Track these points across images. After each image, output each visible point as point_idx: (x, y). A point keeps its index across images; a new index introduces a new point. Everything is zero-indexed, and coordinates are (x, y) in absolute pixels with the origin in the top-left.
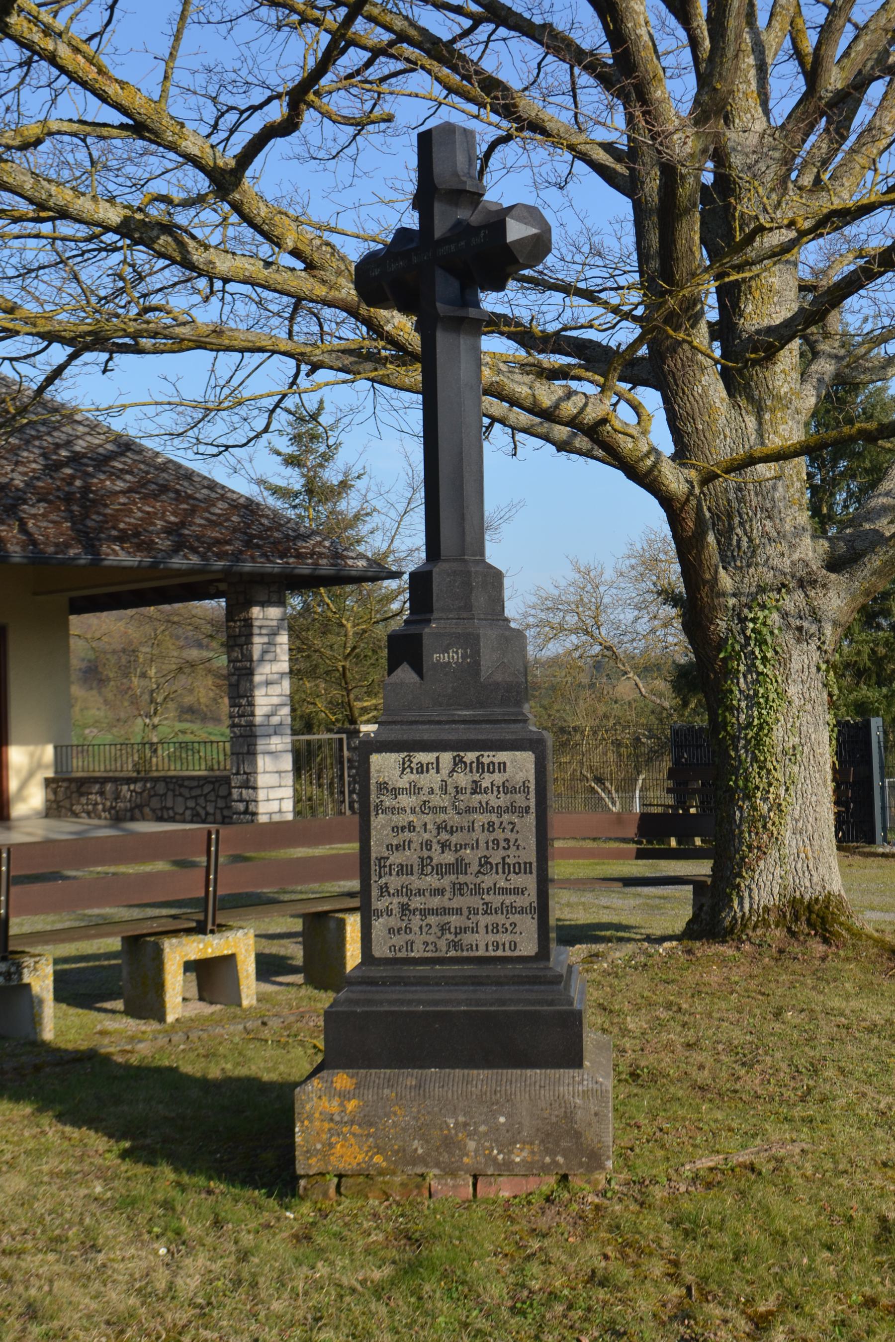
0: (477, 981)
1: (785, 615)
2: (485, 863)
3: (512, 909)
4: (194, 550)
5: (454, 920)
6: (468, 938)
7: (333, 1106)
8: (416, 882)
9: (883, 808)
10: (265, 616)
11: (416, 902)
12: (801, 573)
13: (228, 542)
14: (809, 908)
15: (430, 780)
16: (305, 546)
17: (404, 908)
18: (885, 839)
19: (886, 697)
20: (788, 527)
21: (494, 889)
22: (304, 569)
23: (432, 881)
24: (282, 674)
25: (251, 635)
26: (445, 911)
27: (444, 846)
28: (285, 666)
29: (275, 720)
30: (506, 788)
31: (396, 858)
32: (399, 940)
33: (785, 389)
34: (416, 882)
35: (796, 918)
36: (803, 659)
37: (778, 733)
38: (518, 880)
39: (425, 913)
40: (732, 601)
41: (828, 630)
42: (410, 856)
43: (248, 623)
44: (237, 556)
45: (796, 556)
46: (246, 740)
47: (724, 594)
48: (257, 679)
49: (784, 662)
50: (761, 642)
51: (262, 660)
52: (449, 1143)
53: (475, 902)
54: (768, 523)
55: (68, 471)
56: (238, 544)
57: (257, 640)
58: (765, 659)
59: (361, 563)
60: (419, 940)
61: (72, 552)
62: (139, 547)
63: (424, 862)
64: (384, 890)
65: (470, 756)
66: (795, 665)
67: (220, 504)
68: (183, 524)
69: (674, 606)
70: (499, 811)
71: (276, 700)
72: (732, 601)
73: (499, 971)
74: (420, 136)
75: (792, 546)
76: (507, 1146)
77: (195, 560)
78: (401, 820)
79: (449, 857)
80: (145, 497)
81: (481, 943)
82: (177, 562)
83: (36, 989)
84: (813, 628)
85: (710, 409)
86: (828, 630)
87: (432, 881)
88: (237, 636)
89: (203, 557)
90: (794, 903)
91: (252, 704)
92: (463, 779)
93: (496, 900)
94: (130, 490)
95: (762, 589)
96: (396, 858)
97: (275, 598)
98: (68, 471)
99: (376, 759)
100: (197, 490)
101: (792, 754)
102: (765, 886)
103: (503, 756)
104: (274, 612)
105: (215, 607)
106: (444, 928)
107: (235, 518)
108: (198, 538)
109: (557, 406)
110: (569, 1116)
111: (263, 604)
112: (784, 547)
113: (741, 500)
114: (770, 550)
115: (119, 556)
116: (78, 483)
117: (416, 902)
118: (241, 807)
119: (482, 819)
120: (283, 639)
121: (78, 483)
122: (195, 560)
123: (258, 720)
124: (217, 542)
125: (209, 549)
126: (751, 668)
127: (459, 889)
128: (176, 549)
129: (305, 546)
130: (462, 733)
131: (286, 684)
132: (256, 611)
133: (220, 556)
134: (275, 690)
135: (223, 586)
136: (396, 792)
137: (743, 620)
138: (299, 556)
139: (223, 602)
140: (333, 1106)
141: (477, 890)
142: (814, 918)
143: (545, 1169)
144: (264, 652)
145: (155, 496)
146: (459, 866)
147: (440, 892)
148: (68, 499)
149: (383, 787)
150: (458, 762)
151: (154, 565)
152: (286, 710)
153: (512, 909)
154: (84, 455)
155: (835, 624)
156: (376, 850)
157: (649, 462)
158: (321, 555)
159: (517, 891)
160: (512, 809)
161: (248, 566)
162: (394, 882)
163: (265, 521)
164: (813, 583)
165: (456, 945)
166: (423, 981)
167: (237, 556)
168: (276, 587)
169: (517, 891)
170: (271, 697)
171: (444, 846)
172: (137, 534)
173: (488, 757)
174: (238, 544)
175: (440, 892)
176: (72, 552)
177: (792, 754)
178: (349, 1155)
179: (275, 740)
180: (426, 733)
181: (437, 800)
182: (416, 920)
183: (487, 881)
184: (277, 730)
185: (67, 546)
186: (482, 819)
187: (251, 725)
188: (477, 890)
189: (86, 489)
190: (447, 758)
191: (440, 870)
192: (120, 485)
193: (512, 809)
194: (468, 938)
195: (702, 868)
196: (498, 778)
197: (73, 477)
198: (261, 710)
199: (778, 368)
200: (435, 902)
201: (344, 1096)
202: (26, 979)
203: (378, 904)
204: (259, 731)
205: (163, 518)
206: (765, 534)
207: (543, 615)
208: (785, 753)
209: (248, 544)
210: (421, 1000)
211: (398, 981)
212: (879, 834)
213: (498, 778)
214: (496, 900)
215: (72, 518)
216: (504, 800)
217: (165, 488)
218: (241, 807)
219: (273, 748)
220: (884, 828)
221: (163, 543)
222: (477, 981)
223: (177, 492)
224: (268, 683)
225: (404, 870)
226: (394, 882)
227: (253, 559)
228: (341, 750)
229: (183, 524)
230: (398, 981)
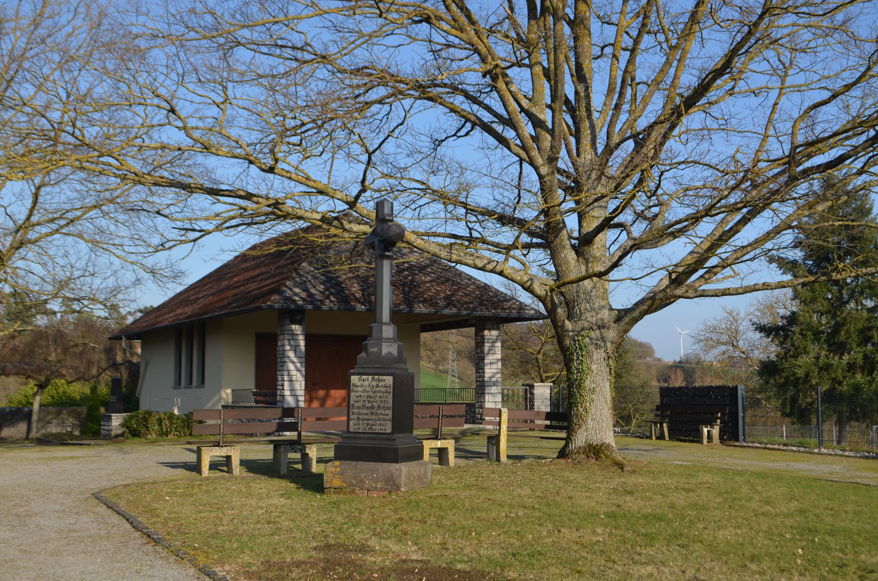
0: (374, 439)
1: (591, 339)
2: (379, 406)
3: (385, 420)
4: (455, 306)
5: (370, 422)
6: (374, 427)
7: (333, 470)
8: (361, 411)
9: (744, 426)
10: (491, 334)
11: (361, 417)
12: (600, 323)
13: (471, 303)
14: (594, 448)
15: (366, 383)
16: (506, 305)
17: (358, 418)
18: (744, 440)
19: (869, 381)
20: (596, 306)
21: (381, 414)
22: (503, 315)
23: (365, 411)
24: (498, 360)
25: (484, 342)
26: (368, 419)
27: (369, 402)
28: (499, 356)
29: (494, 379)
30: (385, 386)
31: (356, 405)
32: (356, 427)
33: (598, 254)
34: (361, 411)
35: (590, 451)
36: (598, 355)
37: (587, 383)
38: (387, 412)
39: (363, 420)
40: (571, 334)
41: (609, 345)
42: (360, 404)
43: (483, 337)
44: (474, 309)
45: (599, 317)
46: (481, 388)
47: (568, 331)
48: (486, 361)
49: (591, 357)
50: (581, 349)
51: (488, 353)
52: (362, 481)
53: (376, 417)
54: (588, 305)
55: (407, 273)
56: (476, 304)
57: (486, 344)
58: (582, 356)
59: (532, 312)
60: (361, 427)
61: (401, 307)
62: (431, 305)
63: (364, 406)
64: (353, 413)
65: (376, 377)
66: (595, 358)
67: (472, 286)
68: (453, 295)
69: (761, 332)
70: (383, 392)
71: (494, 371)
72: (571, 334)
73: (381, 436)
74: (377, 204)
75: (597, 313)
76: (376, 483)
77: (455, 310)
78: (358, 394)
79: (370, 405)
80: (438, 284)
81: (377, 429)
82: (447, 311)
83: (310, 455)
84: (603, 344)
85: (568, 262)
86: (609, 345)
87: (365, 411)
88: (480, 342)
89: (459, 310)
90: (590, 445)
91: (484, 372)
92: (374, 383)
93: (381, 417)
94: (432, 281)
95: (583, 329)
96: (356, 405)
97: (495, 327)
98: (407, 273)
99: (352, 377)
100: (462, 280)
101: (593, 391)
102: (580, 439)
103: (385, 377)
104: (495, 333)
105: (472, 330)
106: (368, 424)
107: (477, 293)
108: (458, 301)
109: (484, 266)
110: (392, 475)
111: (490, 329)
112: (593, 313)
113: (578, 296)
114: (588, 315)
115: (421, 309)
116: (410, 278)
117: (361, 417)
118: (479, 416)
119: (379, 394)
120: (499, 344)
121: (410, 278)
122: (455, 310)
123: (486, 379)
124: (467, 303)
125: (462, 306)
126: (578, 358)
127: (372, 413)
128: (447, 307)
129: (506, 305)
130: (376, 371)
131: (500, 364)
132: (486, 332)
133: (466, 309)
134: (495, 366)
135: (474, 321)
136: (357, 386)
137: (574, 341)
138: (503, 309)
139: (474, 329)
140: (333, 470)
141: (377, 414)
142: (595, 451)
143: (386, 490)
144: (490, 350)
145: (443, 283)
146: (372, 407)
147: (367, 414)
148: (404, 285)
149: (354, 385)
150: (373, 378)
151: (436, 313)
152: (499, 375)
153: (385, 420)
154: (415, 266)
155: (612, 342)
156: (352, 402)
157: (528, 284)
158: (513, 309)
159: (387, 415)
160: (386, 392)
161: (478, 313)
162: (356, 411)
163: (491, 294)
164: (604, 327)
165: (371, 429)
166: (361, 438)
167: (474, 309)
168: (497, 322)
169: (387, 415)
170: (492, 369)
171: (369, 402)
172: (431, 300)
173: (381, 377)
174: (476, 304)
175: (367, 414)
176: (401, 307)
177: (593, 391)
178: (337, 483)
179: (493, 388)
180: (366, 371)
181: (368, 389)
182: (361, 422)
183: (379, 412)
184: (495, 384)
185: (400, 304)
186: (379, 394)
187: (483, 381)
188: (377, 414)
189: (413, 280)
190: (370, 377)
191: (368, 408)
192: (429, 278)
193: (386, 392)
194: (374, 427)
195: (563, 435)
196: (383, 383)
197: (408, 275)
198: (487, 375)
199: (595, 246)
200: (366, 417)
201: (336, 467)
202: (307, 452)
203: (352, 417)
204: (486, 384)
205: (444, 293)
206: (586, 309)
207: (708, 335)
208: (590, 390)
209: (481, 304)
210: (360, 443)
211: (354, 438)
212: (741, 437)
213: (383, 383)
214: (381, 417)
215: (404, 293)
216: (384, 390)
217: (448, 280)
218: (479, 416)
219: (492, 391)
220: (744, 435)
221: (442, 303)
222: (374, 439)
223: (453, 281)
224: (491, 363)
225: (358, 408)
226: (356, 411)
227: (481, 310)
228: (526, 394)
229: (453, 295)
230: (354, 438)
